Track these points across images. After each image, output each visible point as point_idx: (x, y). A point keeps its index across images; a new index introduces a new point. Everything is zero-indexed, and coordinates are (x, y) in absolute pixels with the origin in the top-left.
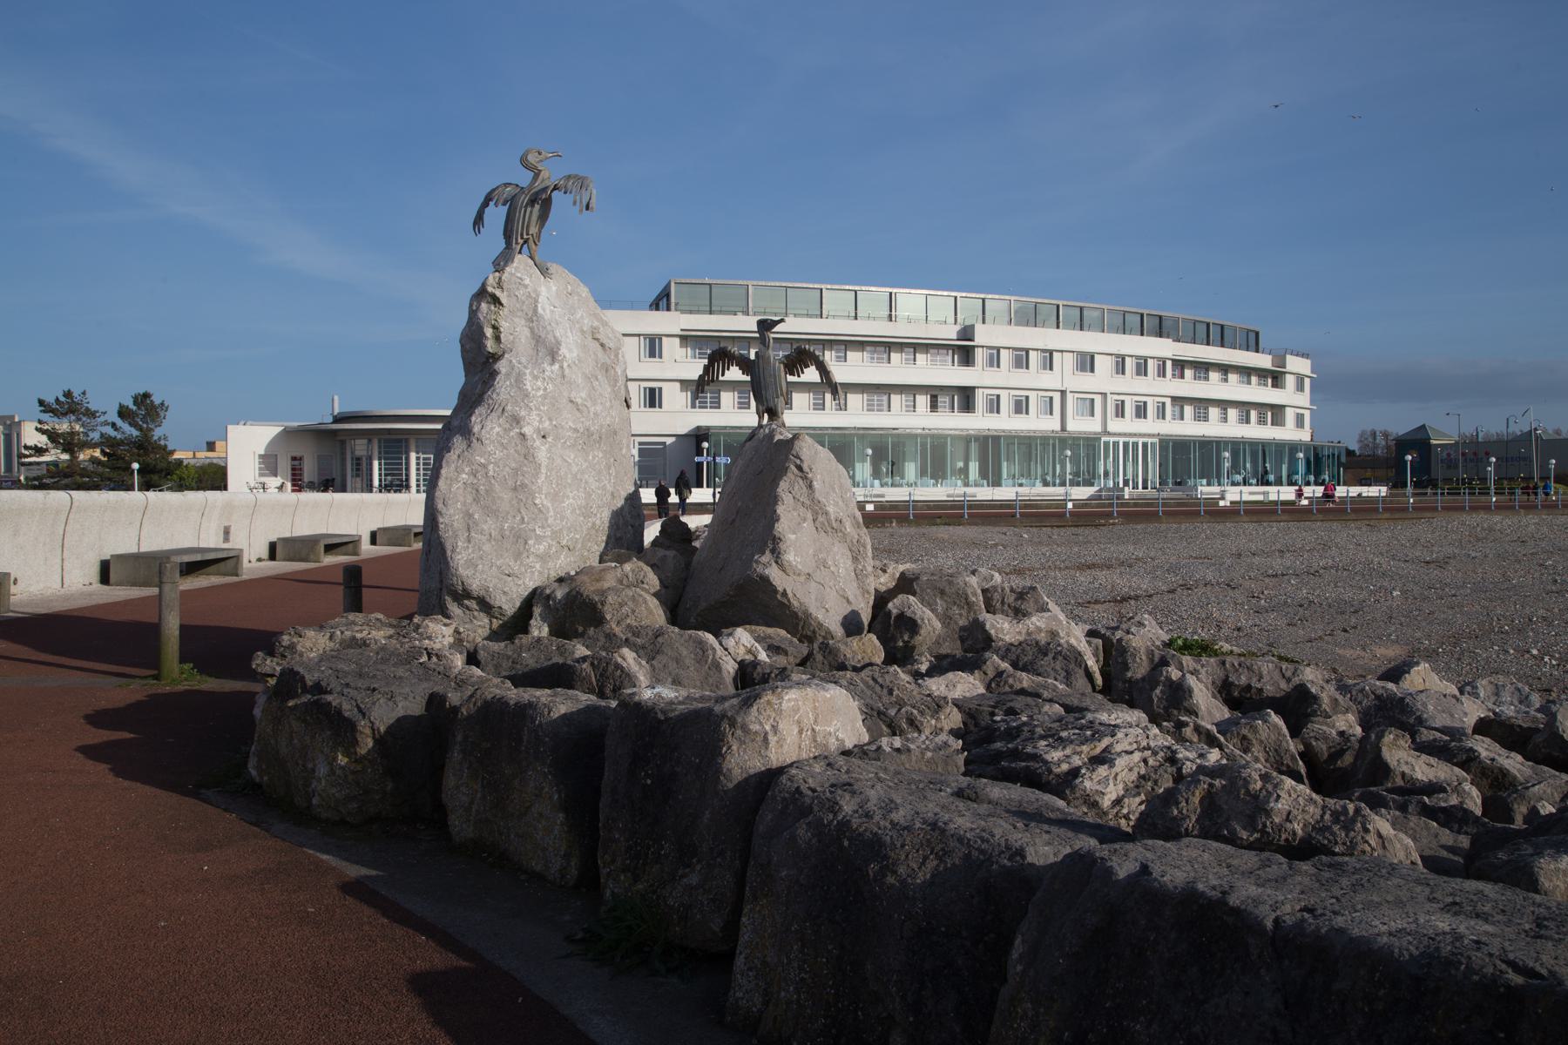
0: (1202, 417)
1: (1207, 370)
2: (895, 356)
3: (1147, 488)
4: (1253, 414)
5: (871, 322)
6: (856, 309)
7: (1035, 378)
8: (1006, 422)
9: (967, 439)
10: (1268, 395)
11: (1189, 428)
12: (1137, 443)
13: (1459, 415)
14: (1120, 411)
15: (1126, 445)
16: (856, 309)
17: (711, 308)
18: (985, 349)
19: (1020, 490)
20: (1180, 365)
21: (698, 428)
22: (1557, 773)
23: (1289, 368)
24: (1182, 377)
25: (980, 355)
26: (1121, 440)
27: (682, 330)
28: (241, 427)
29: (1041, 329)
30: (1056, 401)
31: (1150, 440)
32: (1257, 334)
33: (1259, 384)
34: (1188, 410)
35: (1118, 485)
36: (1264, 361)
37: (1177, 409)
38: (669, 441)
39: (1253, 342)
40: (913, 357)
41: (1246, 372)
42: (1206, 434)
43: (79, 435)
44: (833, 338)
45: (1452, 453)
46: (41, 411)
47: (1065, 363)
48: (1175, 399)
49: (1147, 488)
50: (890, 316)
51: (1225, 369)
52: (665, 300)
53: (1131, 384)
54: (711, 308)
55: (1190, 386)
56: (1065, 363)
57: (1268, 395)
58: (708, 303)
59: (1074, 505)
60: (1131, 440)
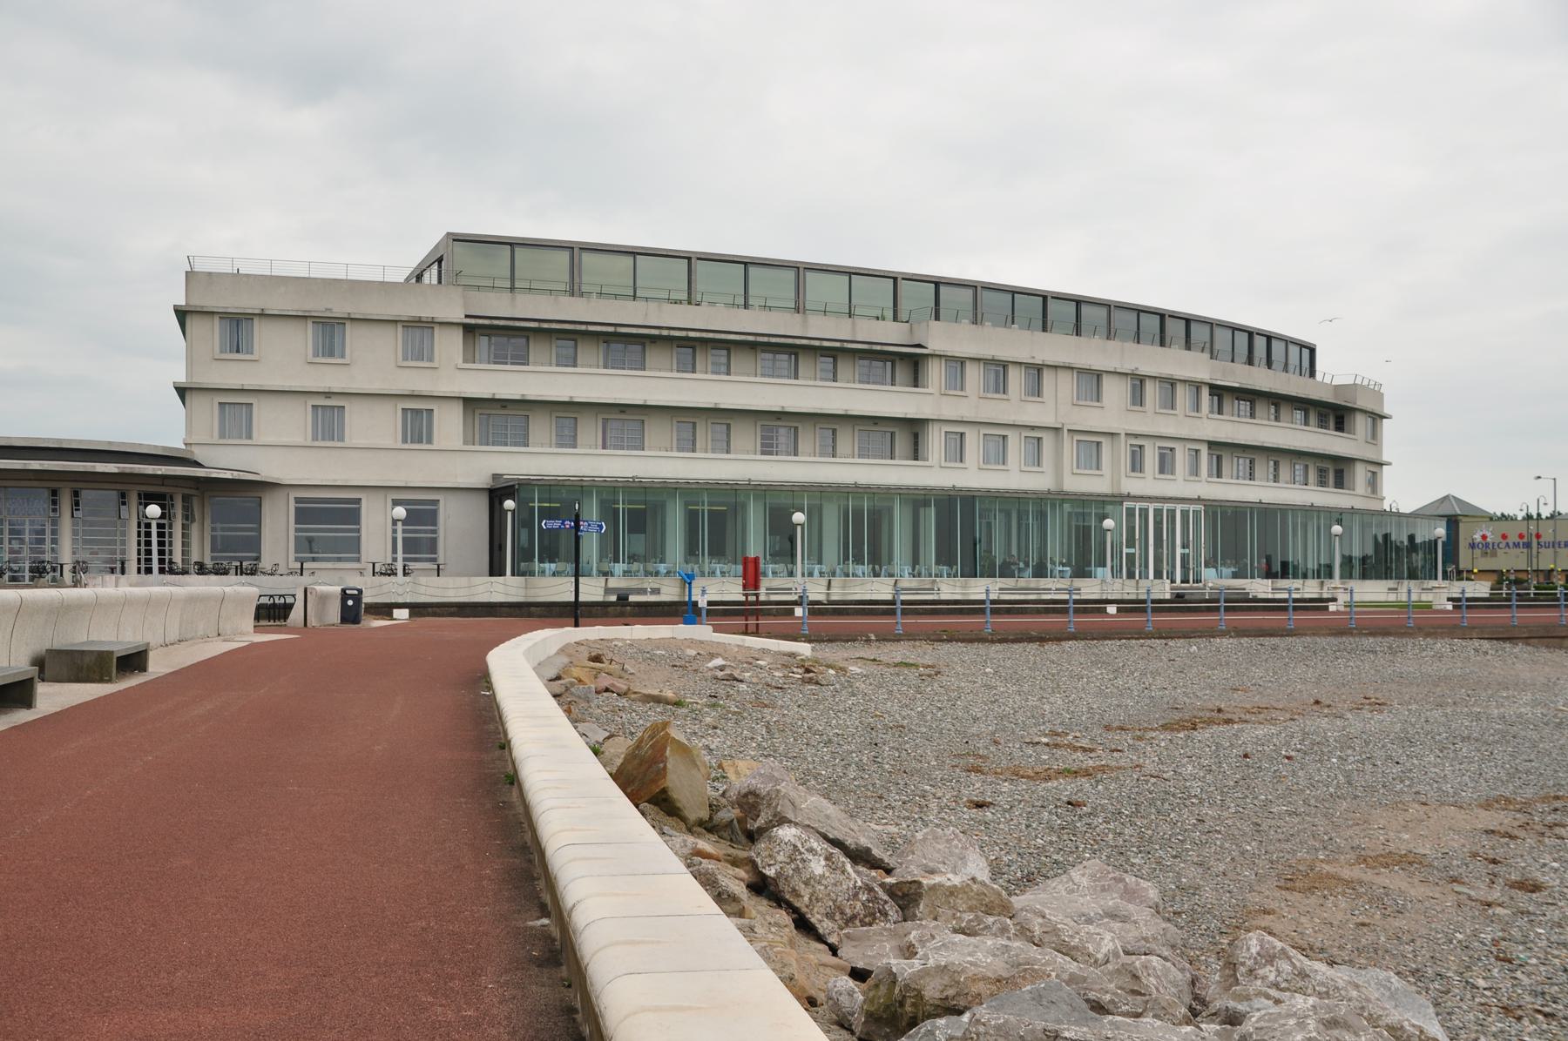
0: (997, 455)
3: (1188, 582)
5: (603, 302)
6: (1013, 313)
7: (1016, 407)
8: (972, 476)
9: (918, 499)
11: (1236, 489)
12: (1174, 511)
13: (1554, 479)
14: (1137, 465)
15: (1158, 512)
16: (1013, 313)
17: (635, 291)
18: (1075, 371)
22: (1098, 1016)
26: (1179, 508)
27: (467, 316)
29: (578, 299)
30: (1092, 443)
31: (1192, 508)
32: (1312, 351)
35: (1474, 603)
43: (1231, 564)
44: (711, 335)
45: (1488, 534)
46: (1376, 537)
47: (1115, 392)
48: (1212, 445)
49: (1188, 582)
50: (850, 313)
52: (435, 266)
53: (1154, 421)
54: (635, 291)
58: (508, 274)
59: (1119, 610)
60: (1166, 506)
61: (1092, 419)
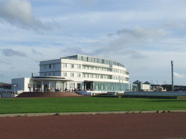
1: (99, 68)
2: (100, 69)
4: (100, 76)
19: (102, 92)
20: (85, 66)
21: (85, 81)
24: (103, 70)
25: (113, 70)
28: (9, 83)
33: (91, 69)
34: (94, 76)
36: (108, 66)
37: (84, 75)
38: (81, 83)
40: (175, 74)
41: (103, 68)
42: (3, 82)
48: (83, 73)
51: (96, 67)
55: (86, 70)
56: (69, 66)
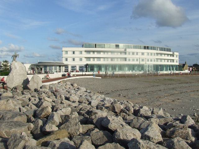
7: (135, 56)
10: (172, 58)
23: (175, 54)
36: (171, 53)
39: (169, 50)
57: (172, 58)
61: (81, 56)
